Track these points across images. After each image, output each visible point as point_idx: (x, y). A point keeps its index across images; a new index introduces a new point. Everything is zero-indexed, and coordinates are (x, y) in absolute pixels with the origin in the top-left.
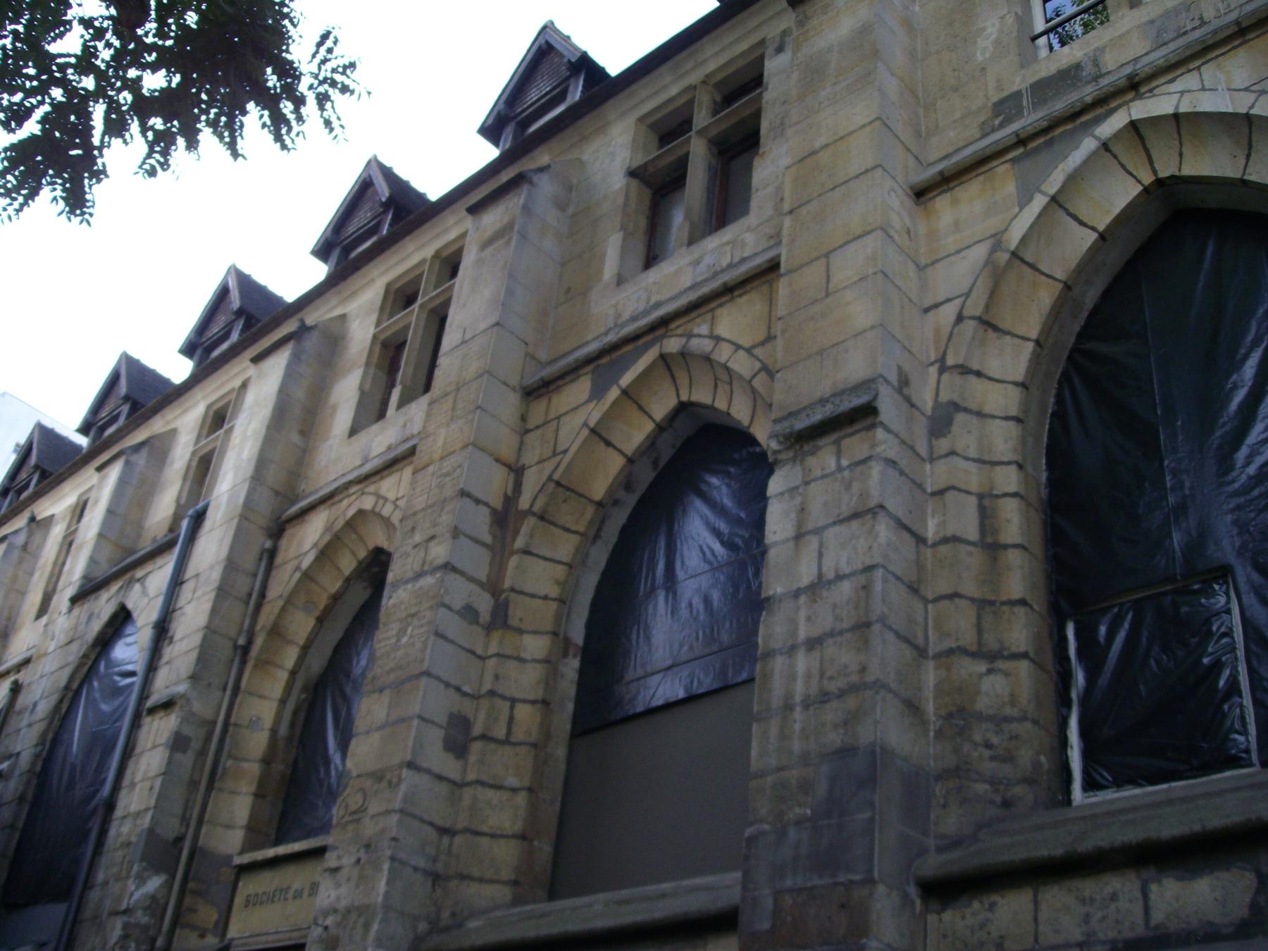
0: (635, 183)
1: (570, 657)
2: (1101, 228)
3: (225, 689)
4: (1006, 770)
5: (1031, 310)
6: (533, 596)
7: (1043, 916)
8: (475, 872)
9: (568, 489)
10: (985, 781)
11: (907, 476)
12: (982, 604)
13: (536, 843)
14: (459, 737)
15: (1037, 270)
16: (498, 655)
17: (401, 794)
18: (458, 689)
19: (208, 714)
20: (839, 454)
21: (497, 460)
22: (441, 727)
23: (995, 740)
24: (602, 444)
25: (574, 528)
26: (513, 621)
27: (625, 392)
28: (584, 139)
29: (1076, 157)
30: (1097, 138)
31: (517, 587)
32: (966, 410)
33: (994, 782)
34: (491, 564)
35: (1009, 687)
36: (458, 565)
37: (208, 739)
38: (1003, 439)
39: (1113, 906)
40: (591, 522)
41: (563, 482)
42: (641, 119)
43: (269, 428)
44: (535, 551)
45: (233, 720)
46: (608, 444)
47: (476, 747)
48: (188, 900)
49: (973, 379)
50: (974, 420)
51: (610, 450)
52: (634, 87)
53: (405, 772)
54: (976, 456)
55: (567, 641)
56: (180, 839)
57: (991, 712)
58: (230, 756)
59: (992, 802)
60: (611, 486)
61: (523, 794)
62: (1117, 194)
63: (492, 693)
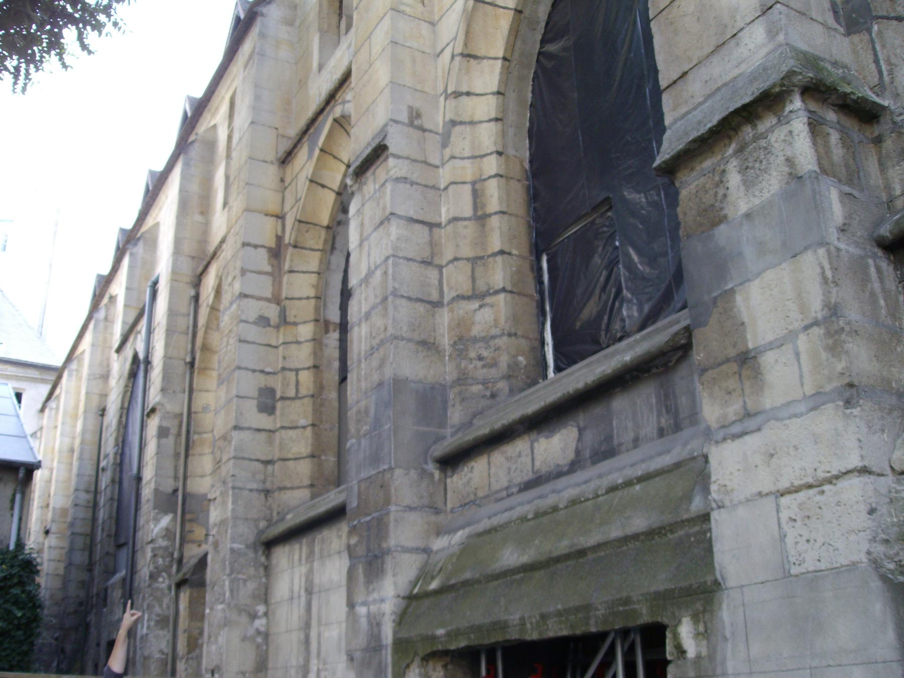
1: (331, 331)
3: (184, 392)
4: (493, 373)
6: (300, 299)
7: (493, 471)
8: (289, 485)
9: (308, 223)
10: (478, 383)
11: (418, 184)
12: (475, 261)
13: (323, 458)
14: (268, 401)
16: (284, 343)
17: (233, 447)
18: (262, 372)
19: (177, 410)
20: (375, 181)
21: (266, 215)
22: (253, 398)
23: (485, 354)
24: (319, 187)
25: (316, 247)
26: (290, 319)
27: (322, 150)
31: (289, 296)
32: (461, 123)
33: (485, 383)
34: (273, 285)
35: (492, 316)
36: (247, 293)
37: (180, 426)
38: (487, 136)
39: (520, 460)
40: (325, 241)
41: (302, 219)
43: (178, 217)
44: (296, 269)
45: (193, 410)
46: (323, 186)
47: (279, 405)
48: (188, 527)
49: (464, 99)
50: (468, 129)
51: (326, 190)
53: (235, 434)
54: (470, 155)
55: (327, 323)
56: (175, 491)
57: (483, 334)
58: (195, 433)
59: (484, 396)
61: (310, 428)
63: (283, 369)
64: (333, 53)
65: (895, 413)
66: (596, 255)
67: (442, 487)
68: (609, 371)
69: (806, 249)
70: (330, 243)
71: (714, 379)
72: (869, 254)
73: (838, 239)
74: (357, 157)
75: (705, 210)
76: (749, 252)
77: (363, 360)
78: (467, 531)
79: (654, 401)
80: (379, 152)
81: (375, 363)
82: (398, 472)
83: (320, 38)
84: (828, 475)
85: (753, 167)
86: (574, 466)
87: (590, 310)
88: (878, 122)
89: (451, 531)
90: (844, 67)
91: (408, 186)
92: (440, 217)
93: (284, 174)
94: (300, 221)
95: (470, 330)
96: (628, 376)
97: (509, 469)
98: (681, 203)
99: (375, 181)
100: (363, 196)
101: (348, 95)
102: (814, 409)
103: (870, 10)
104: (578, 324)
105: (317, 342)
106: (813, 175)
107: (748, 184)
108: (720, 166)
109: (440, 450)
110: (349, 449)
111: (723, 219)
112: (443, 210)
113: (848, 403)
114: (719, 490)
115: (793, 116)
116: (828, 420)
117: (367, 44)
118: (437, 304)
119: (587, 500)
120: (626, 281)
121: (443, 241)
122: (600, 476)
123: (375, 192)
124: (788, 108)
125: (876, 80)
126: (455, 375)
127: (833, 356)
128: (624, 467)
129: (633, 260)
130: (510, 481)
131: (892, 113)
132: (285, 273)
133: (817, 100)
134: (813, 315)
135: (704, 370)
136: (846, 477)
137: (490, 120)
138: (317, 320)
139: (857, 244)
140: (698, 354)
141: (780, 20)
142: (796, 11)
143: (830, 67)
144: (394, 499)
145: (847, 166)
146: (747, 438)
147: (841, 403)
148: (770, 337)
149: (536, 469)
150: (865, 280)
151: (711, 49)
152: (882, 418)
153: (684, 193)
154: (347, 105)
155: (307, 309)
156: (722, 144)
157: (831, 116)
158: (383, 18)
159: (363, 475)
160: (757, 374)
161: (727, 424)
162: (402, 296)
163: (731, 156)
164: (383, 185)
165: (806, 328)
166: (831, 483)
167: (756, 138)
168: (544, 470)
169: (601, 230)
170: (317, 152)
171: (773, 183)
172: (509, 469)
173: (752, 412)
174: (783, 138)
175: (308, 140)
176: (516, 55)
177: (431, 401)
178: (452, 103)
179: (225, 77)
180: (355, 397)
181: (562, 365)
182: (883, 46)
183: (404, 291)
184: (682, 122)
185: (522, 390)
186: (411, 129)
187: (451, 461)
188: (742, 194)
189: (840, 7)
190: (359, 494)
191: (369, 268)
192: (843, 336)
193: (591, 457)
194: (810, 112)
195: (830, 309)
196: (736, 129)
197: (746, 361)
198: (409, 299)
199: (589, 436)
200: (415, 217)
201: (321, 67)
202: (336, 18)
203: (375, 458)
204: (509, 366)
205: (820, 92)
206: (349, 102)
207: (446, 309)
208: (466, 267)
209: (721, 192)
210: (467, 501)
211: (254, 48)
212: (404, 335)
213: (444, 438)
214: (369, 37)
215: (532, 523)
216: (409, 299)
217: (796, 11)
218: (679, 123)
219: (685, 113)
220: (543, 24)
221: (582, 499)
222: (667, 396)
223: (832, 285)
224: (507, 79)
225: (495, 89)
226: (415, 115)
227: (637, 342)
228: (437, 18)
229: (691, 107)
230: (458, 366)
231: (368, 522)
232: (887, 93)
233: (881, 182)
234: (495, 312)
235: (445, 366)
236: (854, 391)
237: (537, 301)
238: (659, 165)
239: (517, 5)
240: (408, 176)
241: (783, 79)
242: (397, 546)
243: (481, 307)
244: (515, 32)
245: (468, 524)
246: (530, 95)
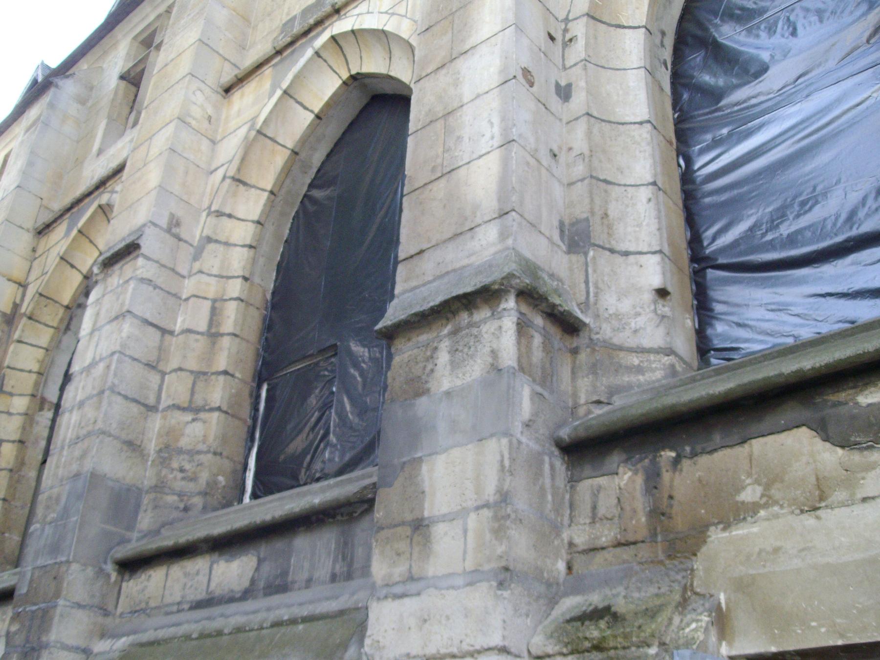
0: (123, 84)
1: (46, 410)
2: (316, 111)
4: (191, 487)
5: (268, 171)
6: (22, 370)
7: (168, 584)
9: (48, 298)
10: (174, 494)
12: (199, 375)
13: (7, 535)
15: (276, 142)
20: (120, 276)
21: (9, 280)
23: (187, 466)
24: (68, 266)
25: (51, 324)
27: (80, 231)
28: (106, 53)
29: (302, 61)
30: (313, 48)
31: (12, 366)
32: (217, 241)
33: (181, 495)
35: (203, 432)
40: (62, 320)
41: (43, 293)
42: (135, 38)
44: (25, 340)
46: (73, 266)
49: (225, 219)
50: (221, 248)
51: (74, 270)
52: (131, 15)
55: (43, 401)
57: (189, 448)
59: (177, 508)
60: (74, 295)
62: (326, 86)
64: (115, 142)
65: (542, 601)
66: (313, 396)
67: (117, 588)
68: (297, 510)
69: (492, 435)
70: (66, 322)
71: (388, 538)
72: (547, 451)
73: (522, 433)
74: (110, 248)
75: (412, 380)
76: (442, 426)
77: (66, 448)
78: (131, 639)
79: (333, 546)
80: (130, 249)
81: (77, 453)
82: (75, 567)
83: (107, 125)
84: (471, 649)
85: (462, 351)
86: (247, 594)
87: (297, 445)
88: (578, 335)
89: (116, 636)
90: (560, 280)
91: (151, 288)
92: (175, 324)
93: (38, 244)
94: (41, 295)
95: (178, 441)
96: (314, 518)
97: (185, 585)
98: (392, 368)
99: (120, 276)
100: (106, 288)
101: (117, 186)
102: (471, 584)
103: (589, 237)
104: (282, 457)
105: (29, 417)
106: (511, 370)
107: (455, 365)
108: (434, 342)
109: (124, 552)
110: (32, 533)
111: (426, 392)
112: (179, 320)
113: (501, 585)
114: (372, 645)
115: (506, 313)
116: (480, 597)
117: (147, 144)
118: (152, 409)
119: (251, 630)
120: (335, 427)
121: (172, 349)
122: (269, 609)
123: (117, 287)
124: (503, 305)
125: (583, 298)
126: (153, 482)
127: (496, 539)
128: (293, 605)
129: (345, 408)
130: (183, 597)
131: (590, 330)
132: (13, 342)
133: (529, 304)
134: (487, 497)
135: (381, 528)
136: (488, 653)
137: (244, 246)
138: (33, 396)
139: (537, 440)
140: (378, 512)
142: (528, 222)
143: (546, 278)
144: (64, 593)
145: (543, 368)
146: (406, 601)
147: (494, 584)
148: (444, 510)
149: (210, 590)
150: (538, 474)
151: (450, 235)
152: (529, 603)
153: (397, 360)
154: (115, 195)
155: (27, 382)
156: (440, 323)
157: (539, 320)
158: (168, 124)
159: (40, 562)
160: (427, 541)
161: (390, 583)
162: (119, 394)
163: (445, 336)
164: (127, 282)
165: (478, 508)
166: (472, 656)
167: (470, 325)
168: (218, 592)
169: (322, 373)
170: (75, 232)
171: (476, 369)
172: (185, 585)
173: (416, 577)
174: (492, 330)
175: (69, 218)
176: (284, 190)
177: (123, 503)
178: (212, 220)
179: (5, 134)
180: (50, 482)
181: (259, 493)
182: (595, 271)
183: (122, 389)
184: (410, 294)
185: (215, 509)
186: (168, 236)
187: (131, 566)
188: (447, 373)
189: (567, 227)
190: (31, 581)
191: (94, 358)
192: (508, 523)
193: (264, 588)
194: (521, 313)
195: (501, 495)
196: (455, 313)
197: (420, 527)
198: (126, 397)
199: (266, 568)
200: (150, 320)
201: (100, 152)
202: (128, 110)
203: (55, 549)
204: (208, 484)
205: (533, 297)
206: (116, 192)
207: (159, 415)
208: (190, 380)
209: (430, 366)
210: (138, 608)
211: (40, 115)
212: (112, 432)
213: (129, 541)
214: (150, 138)
215: (194, 643)
216: (126, 397)
217: (528, 222)
218: (407, 295)
219: (415, 286)
220: (315, 170)
221: (247, 628)
222: (346, 543)
223: (507, 474)
224: (270, 211)
225: (256, 217)
226: (174, 223)
227: (330, 487)
228: (219, 138)
229: (421, 283)
230: (158, 474)
231: (33, 612)
232: (590, 311)
233: (570, 388)
234: (205, 428)
235: (146, 470)
236: (508, 575)
237: (249, 427)
238: (381, 329)
239: (295, 146)
240: (154, 279)
241: (503, 278)
242: (57, 642)
243: (194, 420)
244: (287, 171)
245: (135, 632)
246: (288, 231)
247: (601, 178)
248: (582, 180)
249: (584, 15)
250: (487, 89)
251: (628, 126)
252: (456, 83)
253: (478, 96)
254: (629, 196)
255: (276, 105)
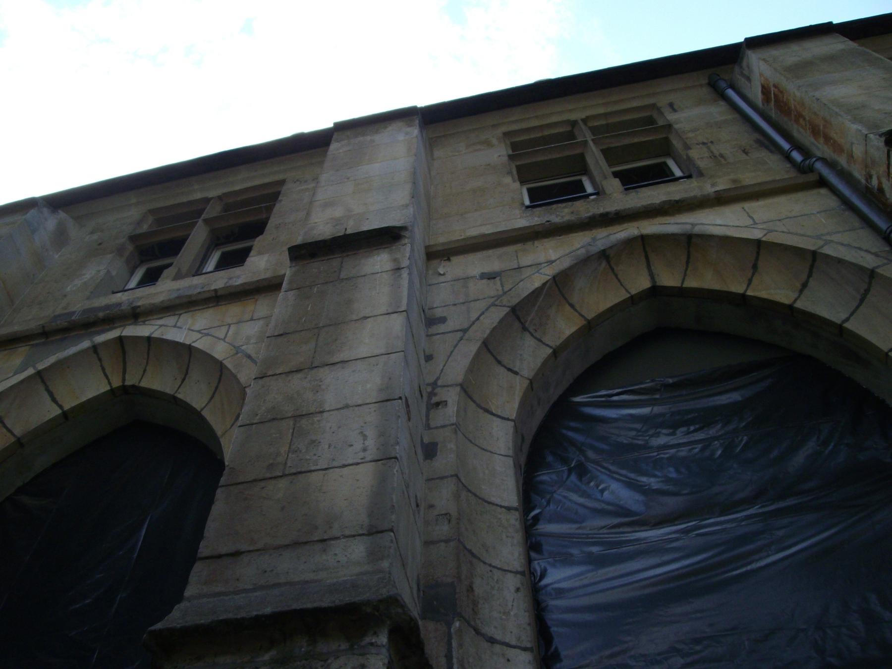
2: (67, 407)
62: (91, 386)
141: (390, 547)
182: (461, 645)
241: (380, 601)
247: (468, 547)
248: (447, 541)
249: (457, 385)
250: (360, 402)
251: (494, 507)
252: (316, 390)
253: (347, 406)
254: (496, 578)
255: (22, 382)
